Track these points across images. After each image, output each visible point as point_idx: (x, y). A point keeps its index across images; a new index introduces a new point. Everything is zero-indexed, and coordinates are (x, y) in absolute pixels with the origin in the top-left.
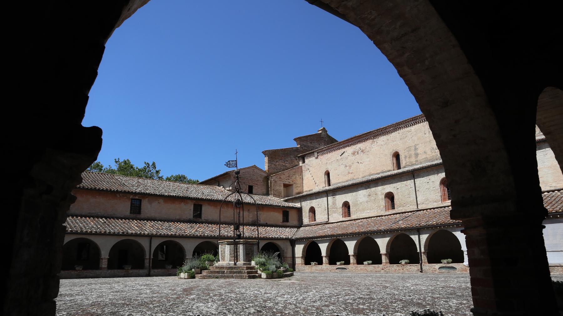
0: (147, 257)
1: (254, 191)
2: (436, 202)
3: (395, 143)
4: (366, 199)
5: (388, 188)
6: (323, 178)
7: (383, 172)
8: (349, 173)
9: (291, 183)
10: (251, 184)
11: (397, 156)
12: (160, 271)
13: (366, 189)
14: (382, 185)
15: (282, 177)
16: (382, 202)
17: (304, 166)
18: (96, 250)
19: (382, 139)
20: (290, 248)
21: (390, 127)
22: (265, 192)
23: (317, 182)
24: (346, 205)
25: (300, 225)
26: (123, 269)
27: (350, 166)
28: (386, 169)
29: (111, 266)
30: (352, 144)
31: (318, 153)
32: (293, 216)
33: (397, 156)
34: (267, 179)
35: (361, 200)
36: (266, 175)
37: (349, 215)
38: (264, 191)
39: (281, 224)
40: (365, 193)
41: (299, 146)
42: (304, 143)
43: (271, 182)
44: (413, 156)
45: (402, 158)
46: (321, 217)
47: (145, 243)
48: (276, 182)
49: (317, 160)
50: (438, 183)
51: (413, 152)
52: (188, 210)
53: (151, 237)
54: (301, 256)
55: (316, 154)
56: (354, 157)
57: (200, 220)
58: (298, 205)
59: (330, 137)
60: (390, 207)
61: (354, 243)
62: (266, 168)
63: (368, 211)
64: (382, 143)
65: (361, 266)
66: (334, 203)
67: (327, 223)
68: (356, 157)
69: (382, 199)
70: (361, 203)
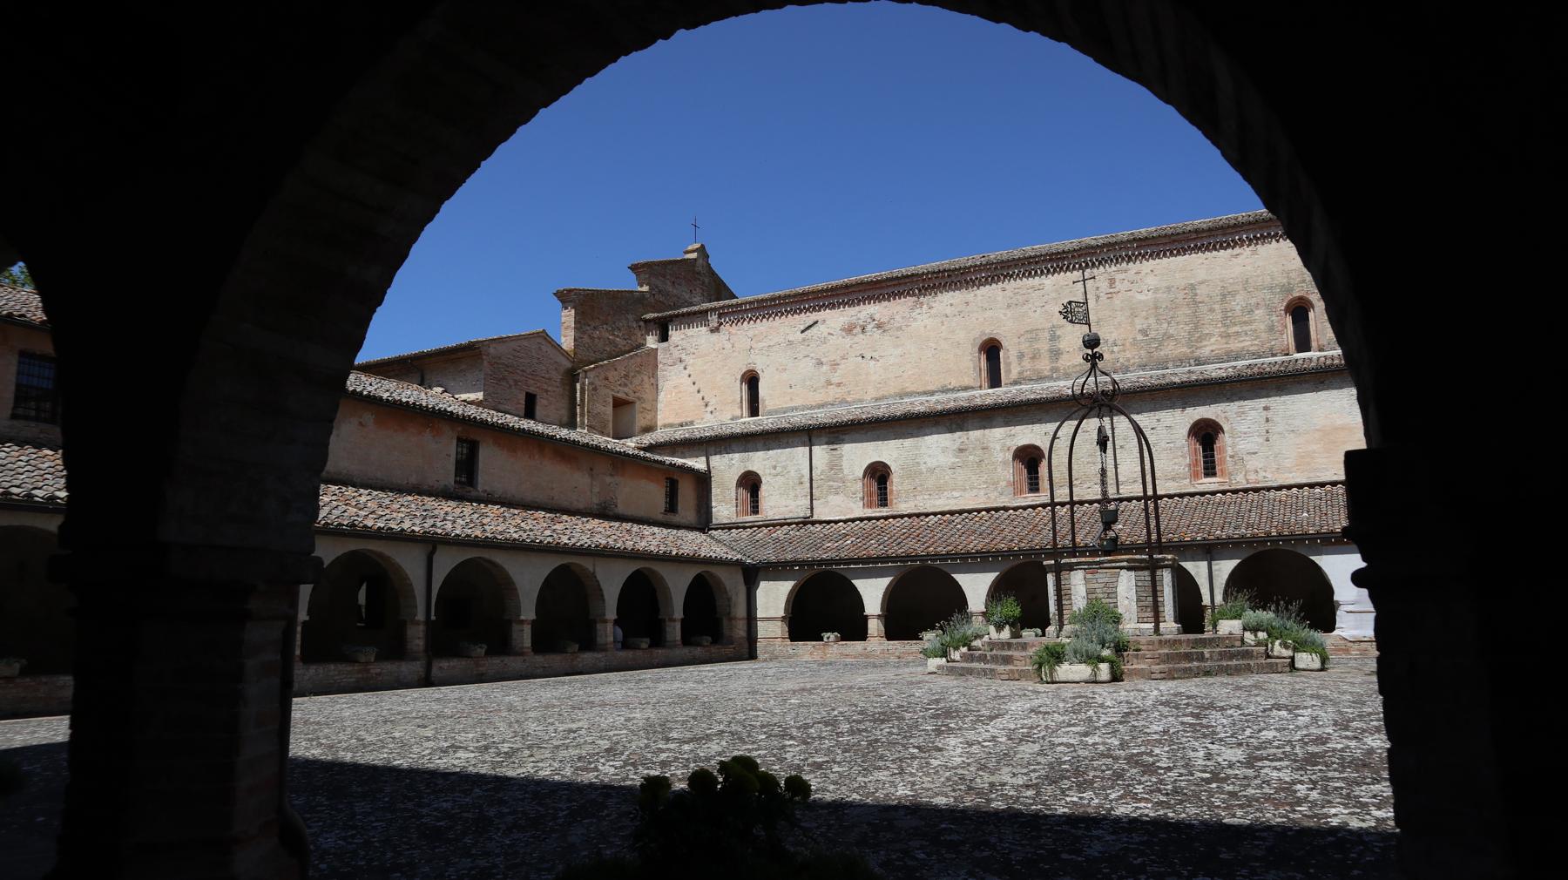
0: (421, 616)
1: (539, 411)
2: (1173, 479)
3: (988, 314)
4: (951, 459)
5: (1034, 434)
6: (739, 392)
7: (945, 391)
8: (829, 383)
9: (630, 398)
10: (532, 390)
11: (991, 350)
12: (333, 670)
13: (951, 431)
14: (1007, 424)
15: (612, 375)
16: (1008, 472)
17: (667, 350)
18: (503, 588)
19: (947, 301)
20: (742, 589)
21: (978, 268)
22: (565, 419)
23: (713, 401)
24: (879, 475)
25: (704, 523)
26: (352, 660)
27: (834, 365)
28: (954, 383)
29: (687, 640)
30: (844, 304)
31: (720, 316)
32: (686, 492)
33: (991, 350)
34: (571, 377)
35: (932, 463)
36: (569, 365)
37: (883, 501)
38: (564, 413)
39: (660, 517)
40: (947, 443)
41: (645, 288)
42: (659, 283)
43: (583, 390)
44: (1046, 355)
45: (1008, 357)
46: (779, 501)
47: (410, 564)
48: (595, 389)
49: (715, 336)
50: (1185, 431)
51: (1044, 346)
52: (443, 453)
53: (432, 543)
54: (782, 613)
55: (713, 319)
56: (848, 340)
57: (474, 493)
58: (698, 463)
59: (713, 273)
60: (1026, 487)
61: (883, 583)
62: (567, 341)
63: (956, 494)
64: (949, 311)
65: (806, 649)
66: (834, 466)
67: (806, 522)
68: (856, 339)
69: (1005, 463)
70: (932, 470)
